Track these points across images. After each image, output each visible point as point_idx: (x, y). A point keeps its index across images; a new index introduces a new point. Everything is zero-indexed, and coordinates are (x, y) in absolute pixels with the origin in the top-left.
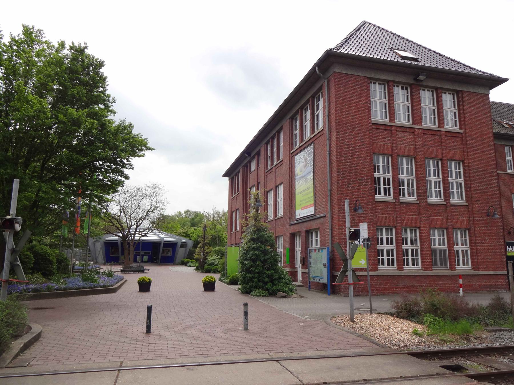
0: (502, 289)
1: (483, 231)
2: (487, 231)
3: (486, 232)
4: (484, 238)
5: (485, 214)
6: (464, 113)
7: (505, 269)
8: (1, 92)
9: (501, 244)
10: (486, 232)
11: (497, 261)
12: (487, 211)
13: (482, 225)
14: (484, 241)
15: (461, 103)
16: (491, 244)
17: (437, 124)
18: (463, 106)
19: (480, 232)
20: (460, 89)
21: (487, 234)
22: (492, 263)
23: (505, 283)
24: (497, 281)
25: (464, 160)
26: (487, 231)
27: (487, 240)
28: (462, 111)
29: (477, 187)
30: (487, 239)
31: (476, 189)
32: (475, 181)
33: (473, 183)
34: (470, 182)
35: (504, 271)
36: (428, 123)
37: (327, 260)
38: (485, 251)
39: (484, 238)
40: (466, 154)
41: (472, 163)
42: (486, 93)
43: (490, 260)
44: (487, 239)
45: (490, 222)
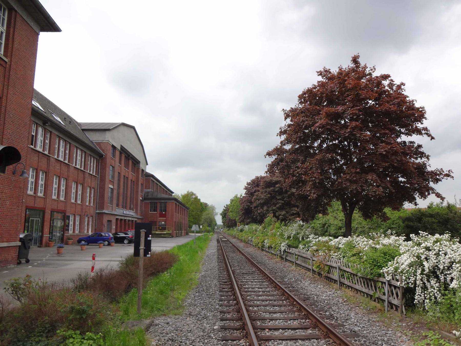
0: (12, 263)
1: (5, 191)
2: (9, 192)
3: (8, 193)
4: (5, 201)
5: (11, 170)
6: (13, 38)
7: (17, 239)
8: (289, 345)
9: (19, 209)
10: (8, 193)
11: (12, 230)
12: (13, 168)
13: (6, 184)
14: (5, 204)
15: (12, 25)
16: (10, 208)
17: (42, 149)
18: (14, 30)
19: (3, 193)
20: (16, 9)
21: (9, 195)
22: (8, 232)
23: (15, 256)
24: (9, 255)
25: (3, 97)
26: (9, 192)
27: (8, 203)
28: (11, 36)
29: (10, 135)
30: (8, 203)
31: (8, 138)
32: (9, 127)
33: (7, 130)
34: (4, 127)
35: (16, 241)
36: (39, 148)
37: (130, 247)
38: (3, 217)
39: (5, 201)
40: (5, 91)
41: (11, 104)
42: (37, 32)
43: (6, 228)
44: (8, 203)
45: (14, 182)
